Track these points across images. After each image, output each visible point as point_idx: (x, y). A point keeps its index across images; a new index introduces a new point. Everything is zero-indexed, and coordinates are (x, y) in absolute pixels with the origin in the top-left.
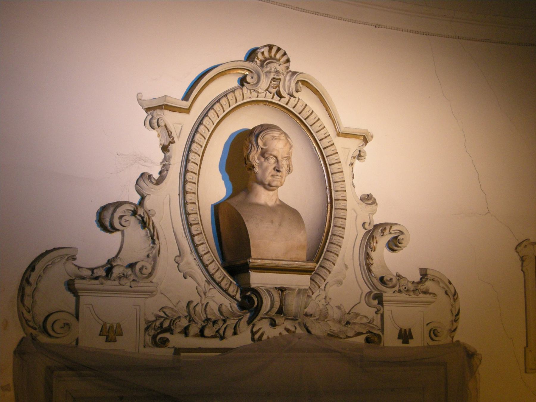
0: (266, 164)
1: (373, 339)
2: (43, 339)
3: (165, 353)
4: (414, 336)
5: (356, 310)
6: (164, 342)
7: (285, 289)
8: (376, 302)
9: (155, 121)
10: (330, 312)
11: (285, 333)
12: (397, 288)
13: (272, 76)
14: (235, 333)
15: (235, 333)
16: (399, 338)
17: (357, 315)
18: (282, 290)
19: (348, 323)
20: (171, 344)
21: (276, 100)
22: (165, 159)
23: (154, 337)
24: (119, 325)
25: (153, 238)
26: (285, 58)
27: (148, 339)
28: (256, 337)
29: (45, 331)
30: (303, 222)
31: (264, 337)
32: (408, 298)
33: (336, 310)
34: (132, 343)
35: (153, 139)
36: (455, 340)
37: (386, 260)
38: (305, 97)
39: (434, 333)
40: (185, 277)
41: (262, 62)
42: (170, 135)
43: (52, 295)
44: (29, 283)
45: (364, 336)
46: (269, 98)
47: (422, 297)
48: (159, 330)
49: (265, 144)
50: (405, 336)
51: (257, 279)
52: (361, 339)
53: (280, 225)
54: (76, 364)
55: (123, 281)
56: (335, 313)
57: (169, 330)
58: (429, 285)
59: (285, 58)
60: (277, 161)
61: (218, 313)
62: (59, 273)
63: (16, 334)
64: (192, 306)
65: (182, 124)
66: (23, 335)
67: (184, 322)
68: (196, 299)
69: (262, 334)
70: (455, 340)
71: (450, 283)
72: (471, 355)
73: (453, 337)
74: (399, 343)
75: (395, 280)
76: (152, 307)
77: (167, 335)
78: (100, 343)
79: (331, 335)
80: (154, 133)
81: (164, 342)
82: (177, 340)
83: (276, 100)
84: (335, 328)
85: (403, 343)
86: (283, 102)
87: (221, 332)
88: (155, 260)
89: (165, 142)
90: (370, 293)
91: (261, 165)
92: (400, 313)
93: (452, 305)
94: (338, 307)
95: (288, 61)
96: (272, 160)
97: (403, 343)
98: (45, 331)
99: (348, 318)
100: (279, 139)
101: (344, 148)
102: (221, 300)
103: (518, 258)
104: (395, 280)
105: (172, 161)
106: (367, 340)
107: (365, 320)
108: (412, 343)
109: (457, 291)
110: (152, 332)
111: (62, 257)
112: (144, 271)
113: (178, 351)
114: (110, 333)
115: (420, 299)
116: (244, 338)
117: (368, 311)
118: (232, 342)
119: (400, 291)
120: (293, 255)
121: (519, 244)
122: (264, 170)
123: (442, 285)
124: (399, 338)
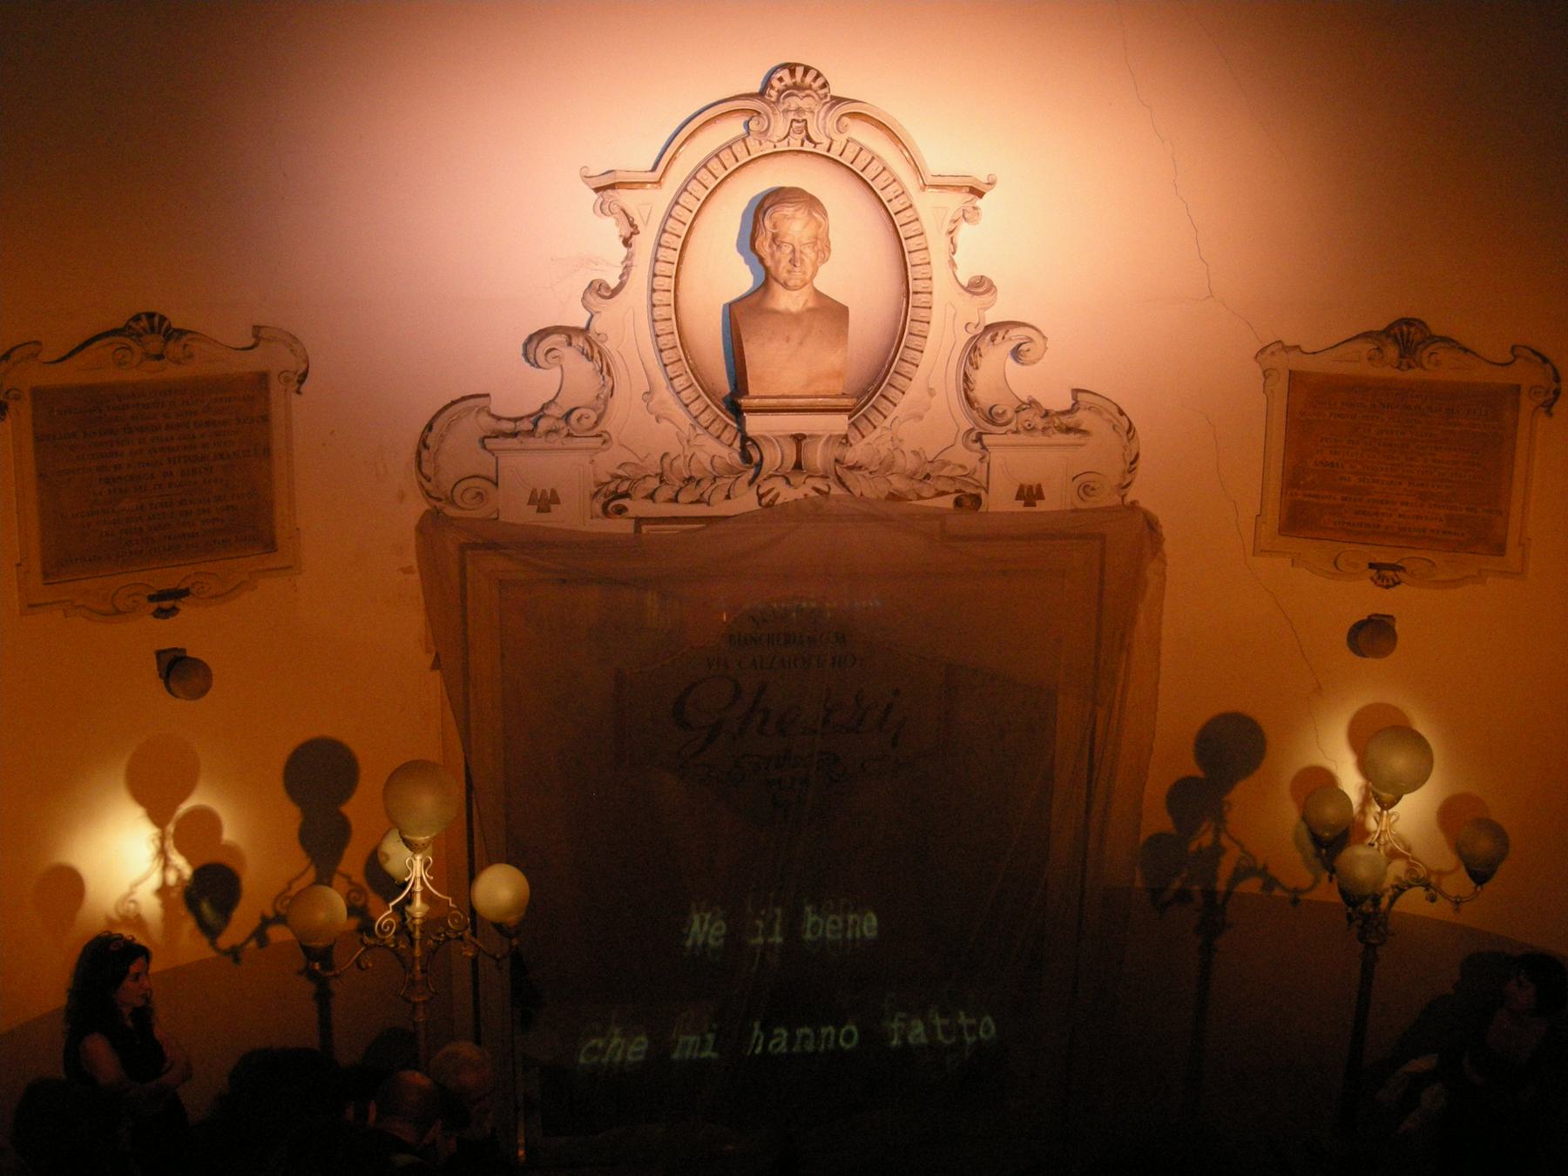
0: (778, 254)
1: (969, 501)
2: (451, 511)
3: (621, 527)
4: (1046, 494)
5: (946, 457)
6: (621, 510)
7: (804, 437)
8: (978, 445)
9: (606, 207)
10: (900, 460)
11: (813, 494)
12: (1012, 426)
13: (791, 116)
14: (728, 497)
15: (728, 497)
16: (1018, 497)
17: (945, 464)
18: (798, 439)
19: (928, 476)
20: (631, 513)
21: (808, 147)
22: (627, 258)
23: (605, 506)
24: (553, 492)
25: (606, 370)
26: (820, 81)
27: (598, 507)
28: (765, 501)
29: (453, 503)
30: (846, 334)
31: (780, 501)
32: (1032, 440)
33: (909, 455)
34: (576, 515)
35: (611, 229)
36: (1128, 499)
37: (1000, 374)
38: (861, 133)
39: (1086, 489)
40: (656, 419)
41: (780, 93)
42: (632, 225)
43: (461, 453)
44: (426, 446)
45: (954, 496)
46: (796, 145)
47: (1072, 438)
48: (612, 498)
49: (775, 226)
50: (1030, 495)
51: (754, 424)
52: (947, 502)
53: (801, 344)
54: (491, 540)
55: (553, 437)
56: (911, 463)
57: (626, 495)
58: (1084, 418)
59: (820, 81)
60: (794, 251)
61: (709, 468)
62: (471, 426)
63: (417, 506)
64: (667, 461)
65: (650, 206)
66: (427, 507)
67: (653, 483)
68: (675, 449)
69: (777, 495)
70: (1128, 499)
71: (1122, 413)
72: (1152, 525)
73: (1123, 497)
74: (1019, 506)
75: (1010, 414)
76: (608, 463)
77: (625, 502)
78: (528, 515)
79: (894, 497)
80: (611, 221)
81: (621, 510)
82: (637, 507)
83: (808, 147)
84: (899, 484)
85: (1026, 505)
86: (821, 150)
87: (706, 496)
88: (606, 402)
89: (627, 231)
90: (972, 430)
91: (772, 255)
92: (1013, 463)
93: (1125, 448)
94: (915, 453)
95: (825, 85)
96: (787, 250)
97: (1026, 505)
98: (453, 503)
99: (928, 468)
100: (793, 218)
101: (932, 209)
102: (716, 450)
103: (1260, 372)
104: (1010, 414)
105: (636, 261)
106: (957, 502)
107: (959, 472)
108: (1041, 506)
109: (1135, 424)
110: (603, 500)
111: (471, 409)
112: (584, 421)
113: (639, 521)
114: (545, 501)
115: (1052, 441)
116: (745, 501)
117: (967, 457)
118: (720, 508)
119: (1016, 432)
120: (821, 388)
121: (1262, 351)
122: (778, 263)
123: (1107, 416)
124: (1018, 497)
